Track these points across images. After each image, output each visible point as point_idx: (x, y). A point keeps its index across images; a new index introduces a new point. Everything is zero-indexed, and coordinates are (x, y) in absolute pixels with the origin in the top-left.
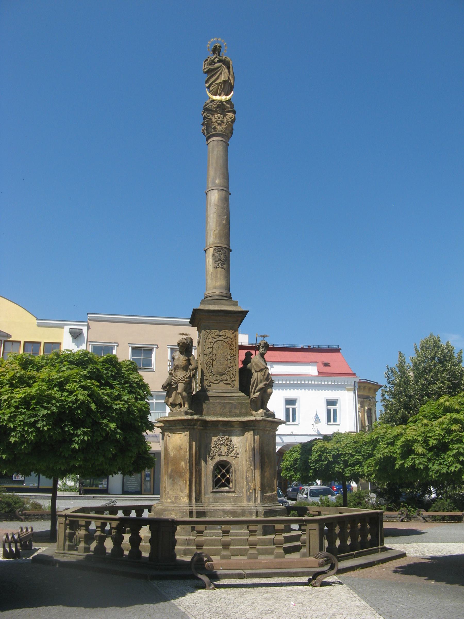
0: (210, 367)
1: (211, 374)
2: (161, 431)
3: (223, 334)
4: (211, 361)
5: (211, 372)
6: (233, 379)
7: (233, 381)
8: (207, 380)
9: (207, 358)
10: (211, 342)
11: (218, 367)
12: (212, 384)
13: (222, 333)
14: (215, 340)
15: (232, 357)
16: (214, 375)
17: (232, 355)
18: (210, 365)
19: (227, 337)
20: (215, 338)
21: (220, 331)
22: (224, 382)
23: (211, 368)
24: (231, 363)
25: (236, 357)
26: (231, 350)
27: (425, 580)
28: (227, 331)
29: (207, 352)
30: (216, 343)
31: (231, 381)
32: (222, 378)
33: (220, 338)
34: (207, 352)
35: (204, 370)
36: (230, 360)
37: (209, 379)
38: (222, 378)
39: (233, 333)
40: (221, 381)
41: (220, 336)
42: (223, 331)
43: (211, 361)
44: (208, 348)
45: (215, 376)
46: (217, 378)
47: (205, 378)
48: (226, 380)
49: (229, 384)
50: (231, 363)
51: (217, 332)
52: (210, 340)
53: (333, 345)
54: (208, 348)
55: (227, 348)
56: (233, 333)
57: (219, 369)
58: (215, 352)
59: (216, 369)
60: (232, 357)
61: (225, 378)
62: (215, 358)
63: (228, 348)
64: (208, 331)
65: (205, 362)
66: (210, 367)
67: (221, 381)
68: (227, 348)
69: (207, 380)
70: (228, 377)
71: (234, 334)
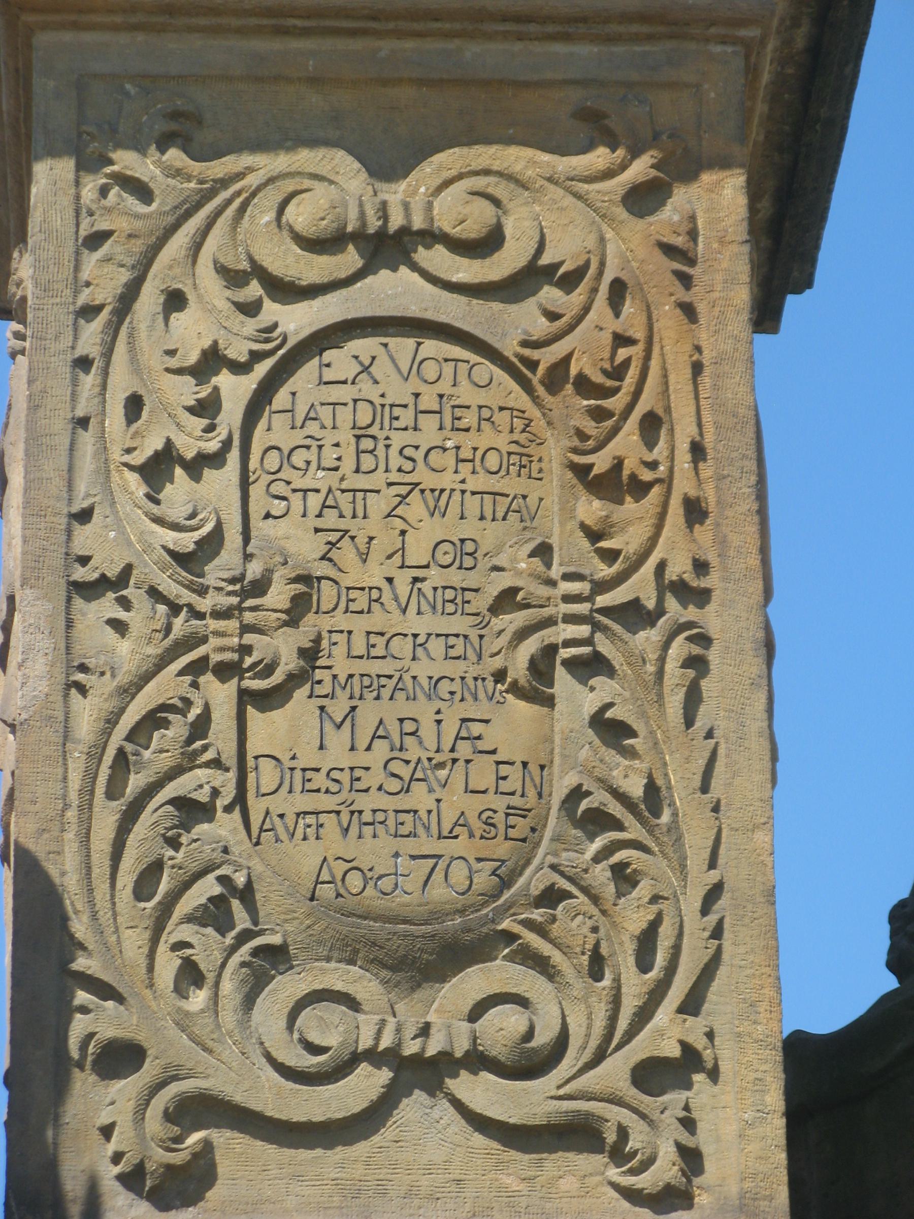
0: (191, 810)
1: (207, 945)
2: (77, 1070)
3: (458, 212)
4: (220, 695)
5: (215, 915)
6: (665, 1034)
7: (653, 1075)
8: (120, 1058)
9: (127, 653)
10: (212, 361)
11: (353, 821)
12: (229, 1144)
13: (437, 191)
14: (297, 320)
15: (634, 615)
16: (276, 957)
17: (641, 586)
18: (194, 783)
19: (531, 277)
20: (286, 291)
21: (386, 167)
22: (482, 1092)
23: (224, 827)
24: (610, 730)
25: (711, 618)
26: (612, 485)
27: (561, 263)
28: (517, 158)
29: (131, 533)
30: (304, 378)
31: (616, 1071)
32: (443, 1014)
33: (394, 290)
34: (131, 533)
35: (65, 871)
36: (591, 666)
37: (166, 1045)
38: (443, 1014)
39: (643, 199)
40: (422, 1073)
41: (387, 247)
42: (449, 160)
43: (220, 695)
44: (157, 469)
45: (286, 988)
46: (330, 1029)
47: (93, 1023)
48: (529, 1065)
49: (574, 1134)
50: (610, 730)
51: (335, 185)
52: (192, 332)
53: (467, 404)
54: (157, 469)
55: (523, 460)
56: (643, 199)
57: (374, 851)
58: (293, 538)
59: (305, 858)
60: (634, 615)
61: (502, 1028)
62: (284, 647)
63: (554, 451)
64: (144, 166)
65: (86, 714)
66: (191, 810)
67: (422, 1073)
68: (523, 460)
69: (120, 1058)
70: (561, 1007)
71: (671, 213)
